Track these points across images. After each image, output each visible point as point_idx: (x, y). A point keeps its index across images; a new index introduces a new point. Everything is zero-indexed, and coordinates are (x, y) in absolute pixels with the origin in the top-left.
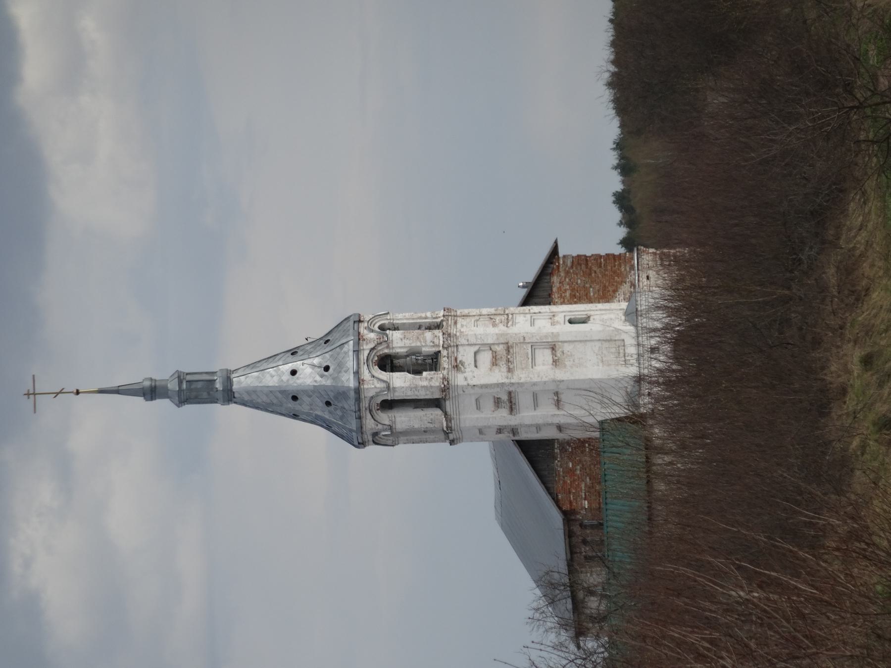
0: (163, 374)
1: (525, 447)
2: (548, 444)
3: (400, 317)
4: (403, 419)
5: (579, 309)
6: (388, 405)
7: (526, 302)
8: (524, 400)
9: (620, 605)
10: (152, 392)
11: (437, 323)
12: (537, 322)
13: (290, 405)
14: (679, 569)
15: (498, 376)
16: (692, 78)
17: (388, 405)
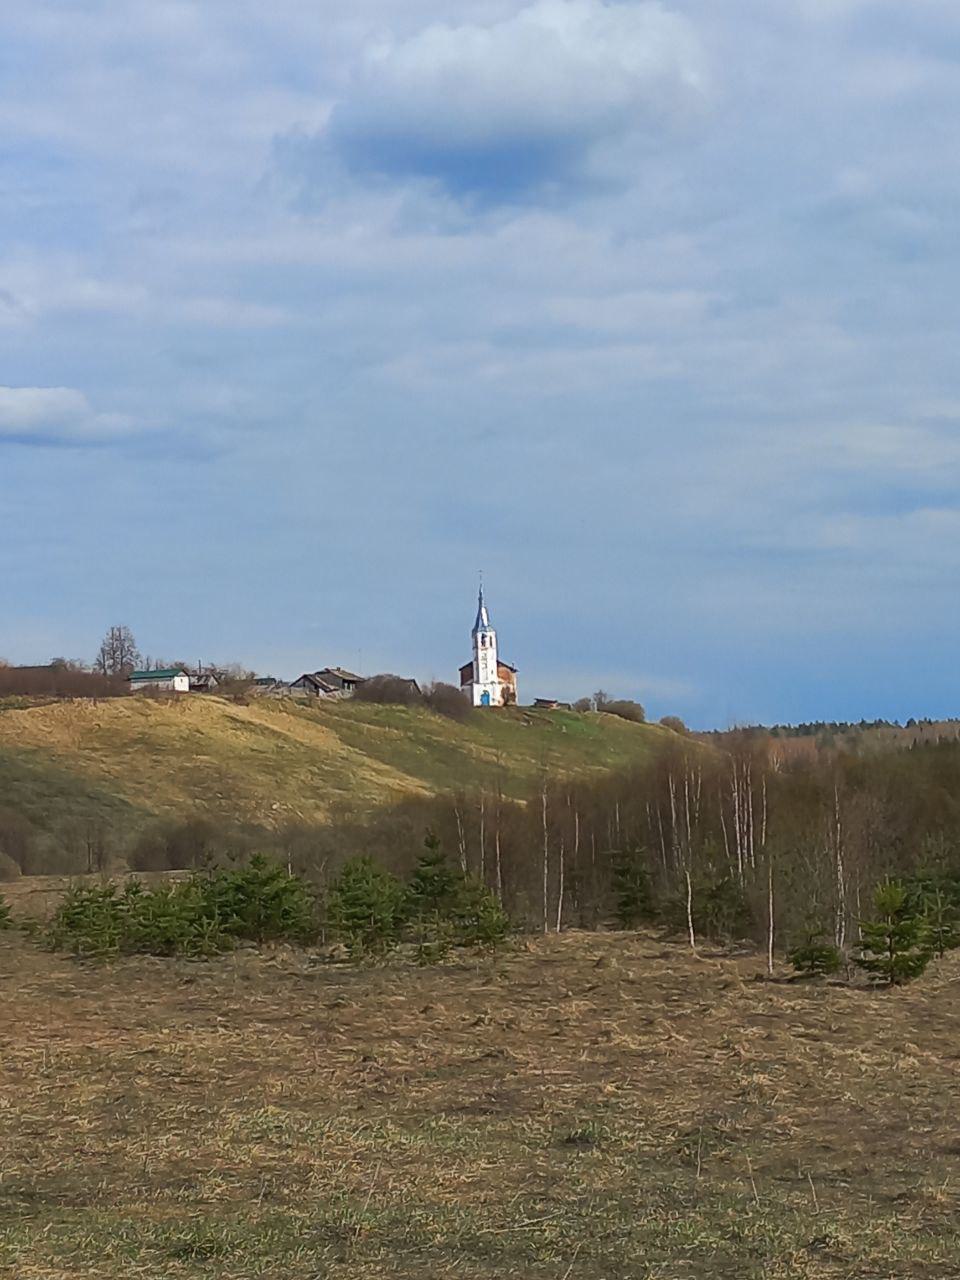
7: (498, 662)
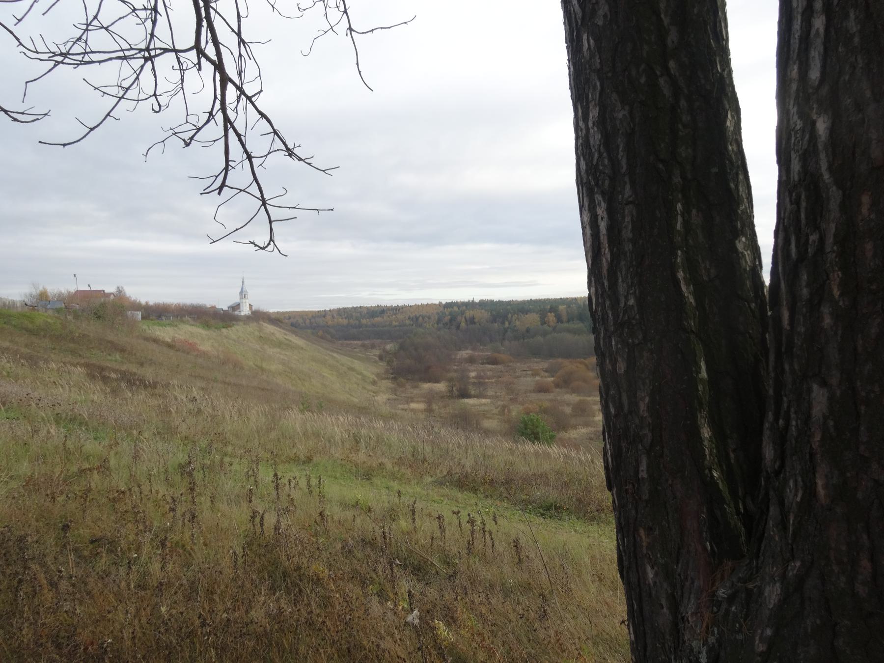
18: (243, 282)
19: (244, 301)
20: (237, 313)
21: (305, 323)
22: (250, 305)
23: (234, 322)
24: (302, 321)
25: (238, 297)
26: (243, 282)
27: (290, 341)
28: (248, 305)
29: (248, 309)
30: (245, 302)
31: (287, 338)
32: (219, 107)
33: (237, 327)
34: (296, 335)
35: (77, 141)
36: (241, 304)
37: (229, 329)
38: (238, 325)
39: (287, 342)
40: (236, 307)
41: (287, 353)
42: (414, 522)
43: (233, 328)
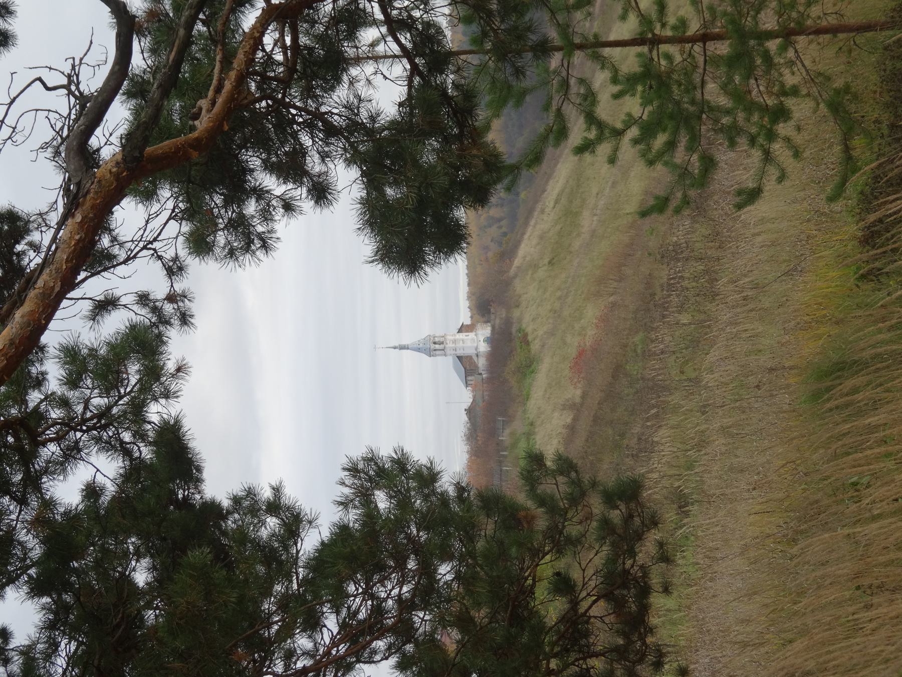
0: (397, 345)
1: (458, 357)
2: (462, 357)
3: (437, 335)
4: (437, 352)
5: (467, 334)
6: (435, 350)
8: (458, 349)
9: (355, 50)
10: (395, 348)
11: (655, 29)
12: (480, 372)
13: (602, 202)
14: (323, 96)
15: (453, 345)
16: (737, 79)
17: (435, 350)
18: (402, 348)
19: (450, 345)
20: (482, 363)
21: (500, 220)
22: (460, 331)
23: (514, 330)
24: (494, 228)
25: (440, 359)
26: (402, 348)
27: (560, 195)
28: (462, 336)
29: (472, 335)
30: (455, 341)
31: (552, 204)
32: (65, 301)
33: (527, 318)
34: (544, 191)
35: (88, 50)
36: (460, 352)
37: (530, 338)
38: (520, 320)
39: (564, 201)
40: (466, 364)
41: (595, 190)
42: (823, 564)
43: (529, 330)
